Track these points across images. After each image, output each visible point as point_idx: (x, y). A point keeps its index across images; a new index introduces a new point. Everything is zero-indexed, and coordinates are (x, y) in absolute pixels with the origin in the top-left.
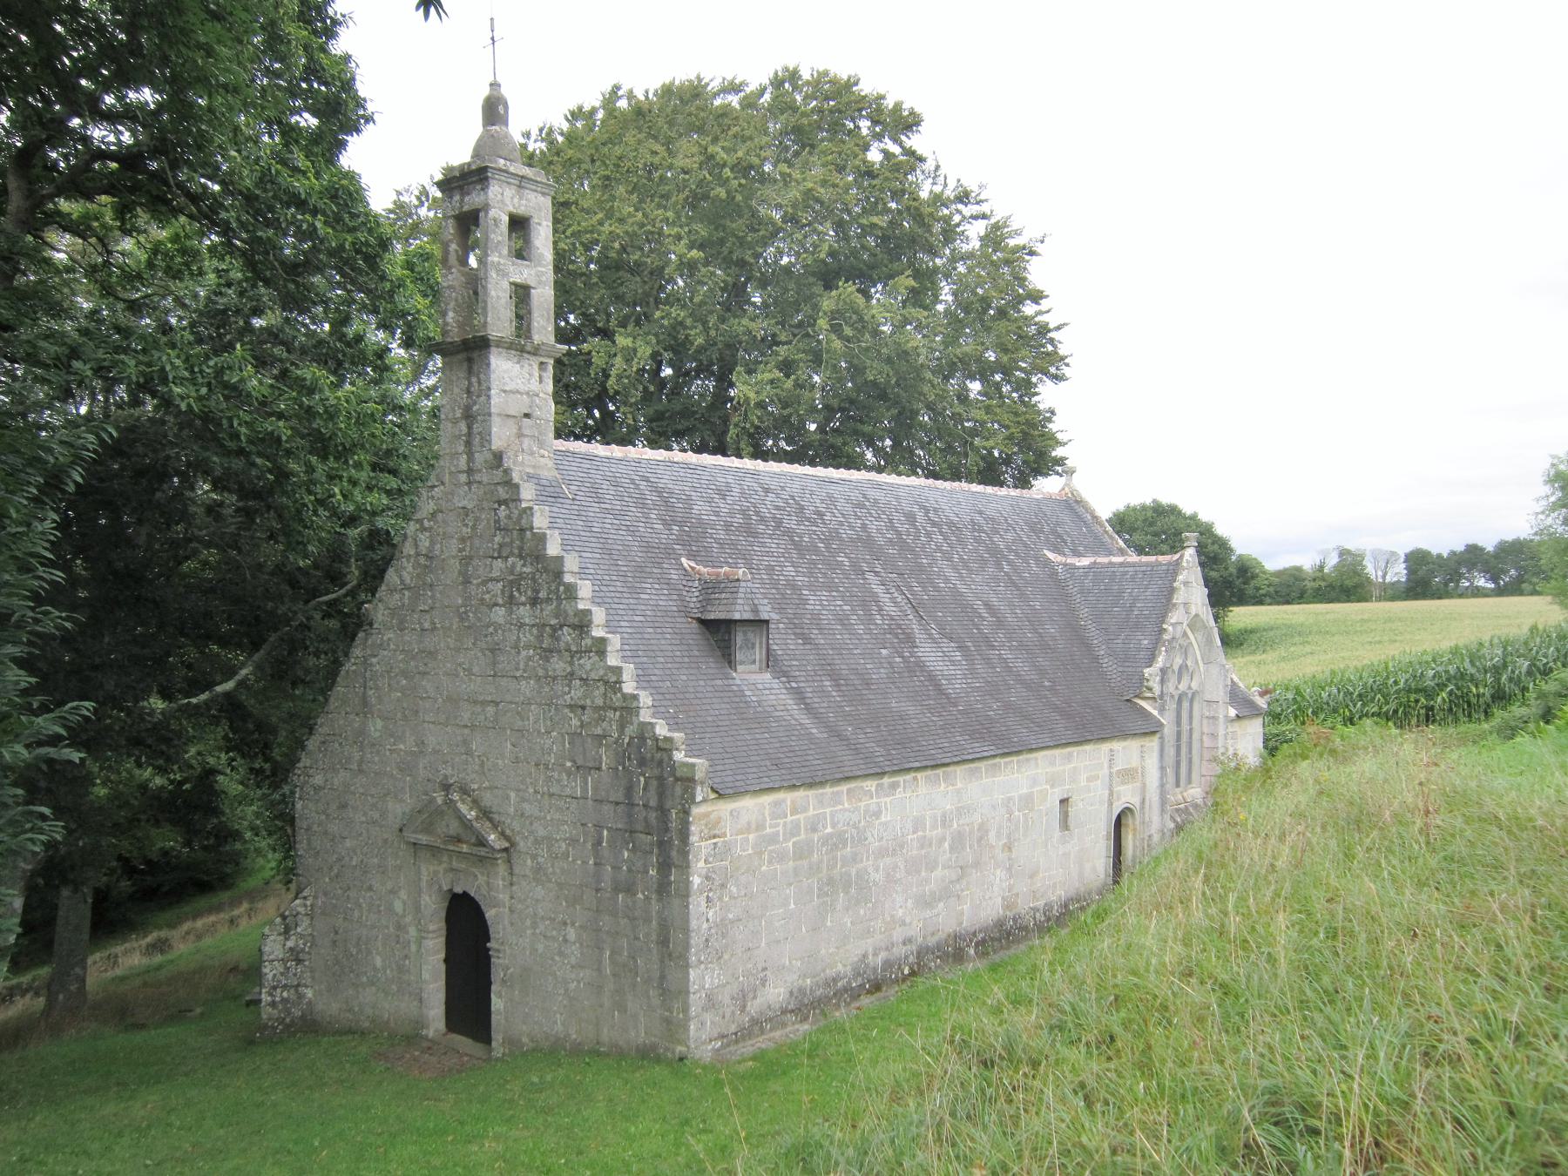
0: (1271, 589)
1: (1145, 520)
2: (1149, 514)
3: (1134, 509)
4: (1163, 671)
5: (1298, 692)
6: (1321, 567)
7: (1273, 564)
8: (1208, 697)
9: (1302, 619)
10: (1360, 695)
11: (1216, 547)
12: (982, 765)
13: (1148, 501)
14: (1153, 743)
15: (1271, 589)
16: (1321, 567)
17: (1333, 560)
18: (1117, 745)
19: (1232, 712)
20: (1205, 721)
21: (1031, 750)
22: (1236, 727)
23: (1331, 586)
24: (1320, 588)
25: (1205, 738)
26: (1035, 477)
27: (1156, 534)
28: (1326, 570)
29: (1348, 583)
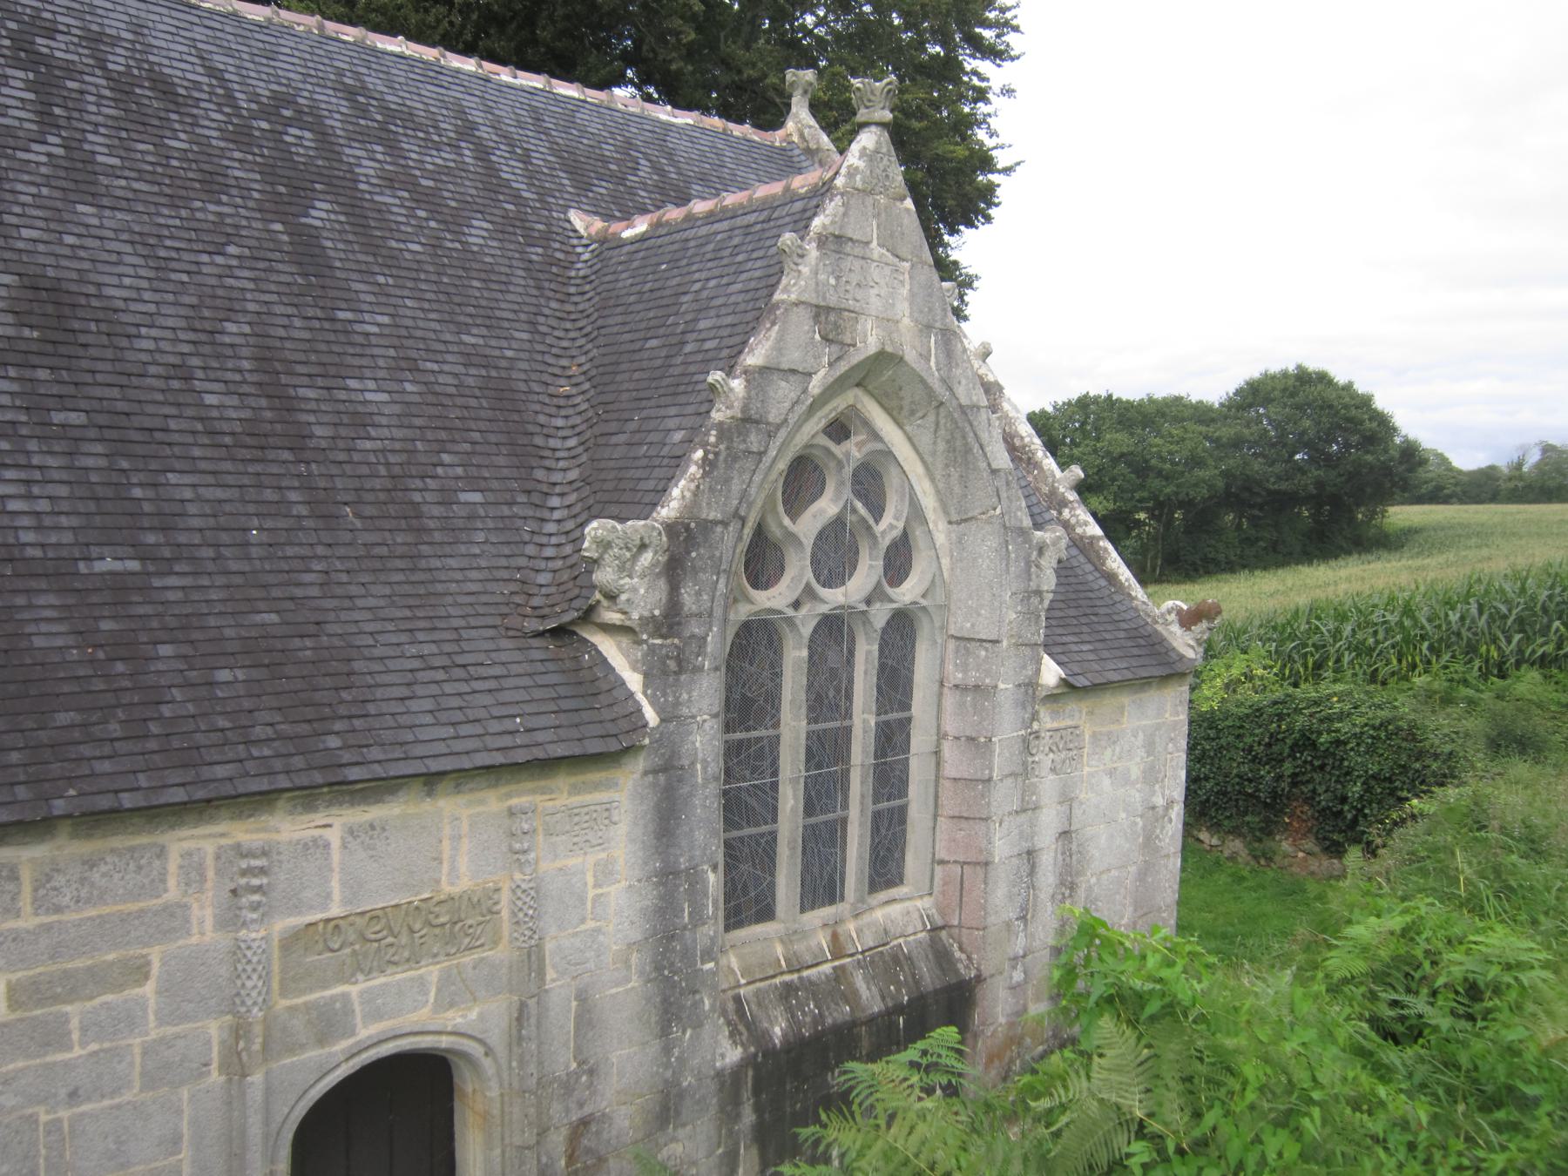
0: (1458, 489)
1: (1285, 390)
2: (1291, 382)
3: (1273, 377)
4: (684, 539)
5: (1408, 611)
6: (1520, 465)
7: (1466, 460)
8: (960, 623)
9: (1485, 517)
10: (1520, 621)
11: (1375, 424)
12: (446, 784)
13: (1291, 368)
14: (623, 796)
15: (1458, 489)
16: (1520, 465)
17: (1534, 457)
18: (286, 829)
19: (1051, 673)
20: (950, 700)
21: (431, 781)
22: (1076, 713)
23: (1529, 487)
24: (1516, 488)
25: (947, 748)
26: (953, 231)
27: (1299, 407)
28: (1525, 469)
29: (1551, 484)
